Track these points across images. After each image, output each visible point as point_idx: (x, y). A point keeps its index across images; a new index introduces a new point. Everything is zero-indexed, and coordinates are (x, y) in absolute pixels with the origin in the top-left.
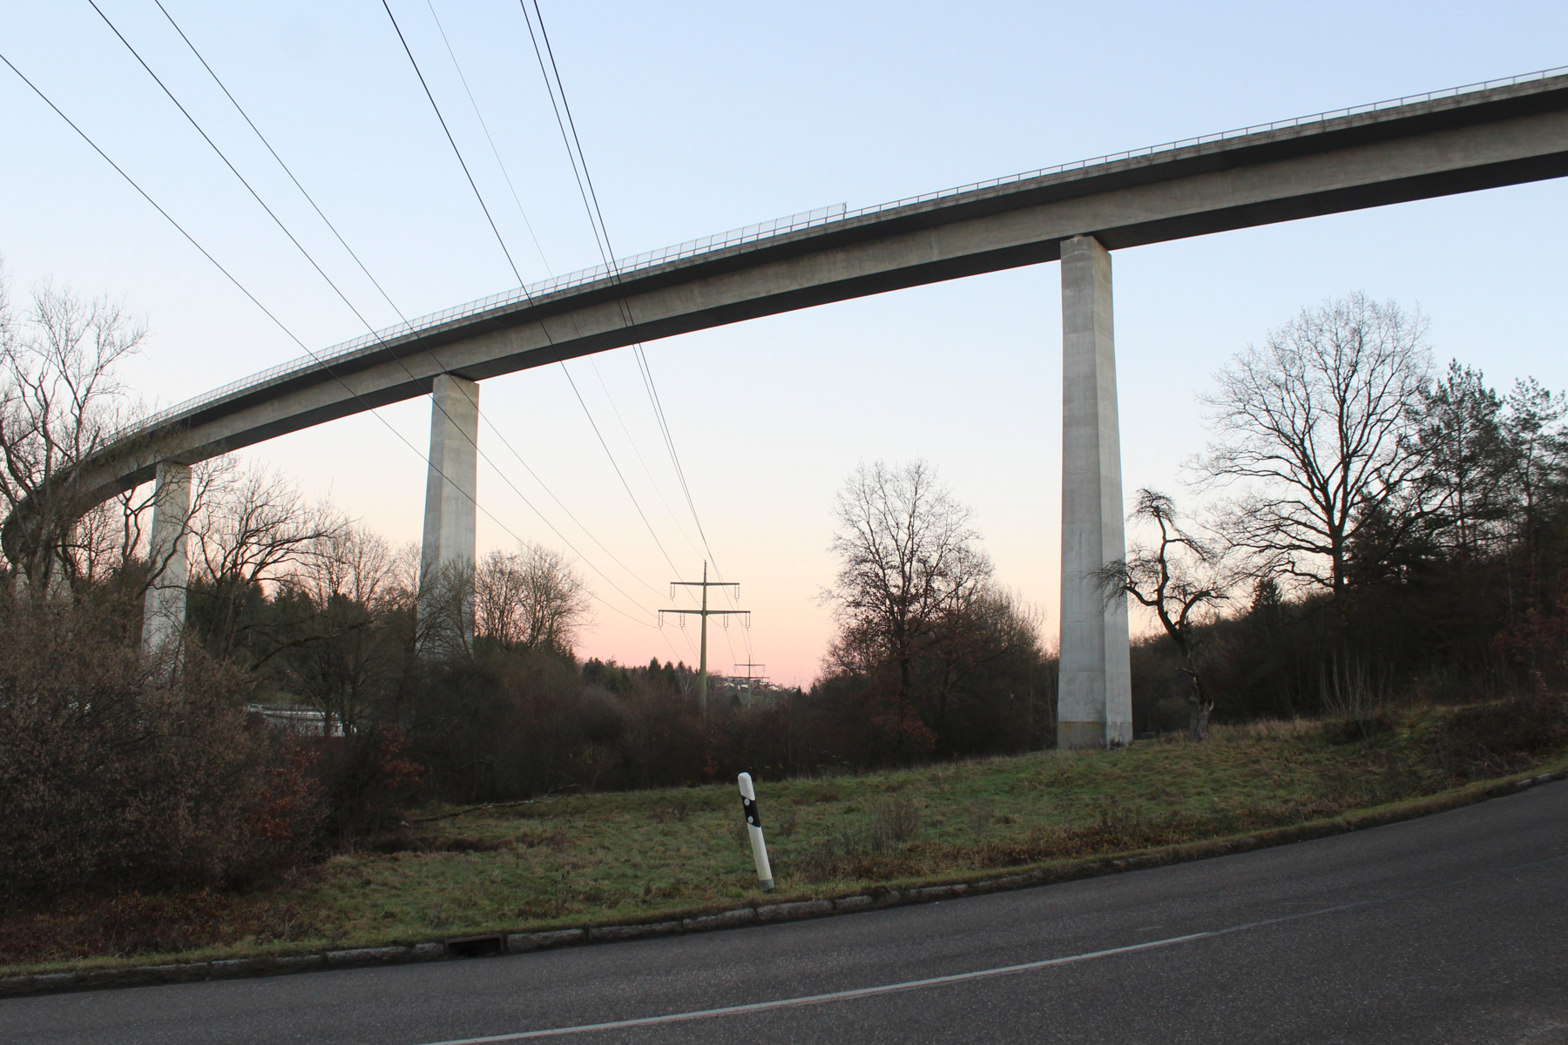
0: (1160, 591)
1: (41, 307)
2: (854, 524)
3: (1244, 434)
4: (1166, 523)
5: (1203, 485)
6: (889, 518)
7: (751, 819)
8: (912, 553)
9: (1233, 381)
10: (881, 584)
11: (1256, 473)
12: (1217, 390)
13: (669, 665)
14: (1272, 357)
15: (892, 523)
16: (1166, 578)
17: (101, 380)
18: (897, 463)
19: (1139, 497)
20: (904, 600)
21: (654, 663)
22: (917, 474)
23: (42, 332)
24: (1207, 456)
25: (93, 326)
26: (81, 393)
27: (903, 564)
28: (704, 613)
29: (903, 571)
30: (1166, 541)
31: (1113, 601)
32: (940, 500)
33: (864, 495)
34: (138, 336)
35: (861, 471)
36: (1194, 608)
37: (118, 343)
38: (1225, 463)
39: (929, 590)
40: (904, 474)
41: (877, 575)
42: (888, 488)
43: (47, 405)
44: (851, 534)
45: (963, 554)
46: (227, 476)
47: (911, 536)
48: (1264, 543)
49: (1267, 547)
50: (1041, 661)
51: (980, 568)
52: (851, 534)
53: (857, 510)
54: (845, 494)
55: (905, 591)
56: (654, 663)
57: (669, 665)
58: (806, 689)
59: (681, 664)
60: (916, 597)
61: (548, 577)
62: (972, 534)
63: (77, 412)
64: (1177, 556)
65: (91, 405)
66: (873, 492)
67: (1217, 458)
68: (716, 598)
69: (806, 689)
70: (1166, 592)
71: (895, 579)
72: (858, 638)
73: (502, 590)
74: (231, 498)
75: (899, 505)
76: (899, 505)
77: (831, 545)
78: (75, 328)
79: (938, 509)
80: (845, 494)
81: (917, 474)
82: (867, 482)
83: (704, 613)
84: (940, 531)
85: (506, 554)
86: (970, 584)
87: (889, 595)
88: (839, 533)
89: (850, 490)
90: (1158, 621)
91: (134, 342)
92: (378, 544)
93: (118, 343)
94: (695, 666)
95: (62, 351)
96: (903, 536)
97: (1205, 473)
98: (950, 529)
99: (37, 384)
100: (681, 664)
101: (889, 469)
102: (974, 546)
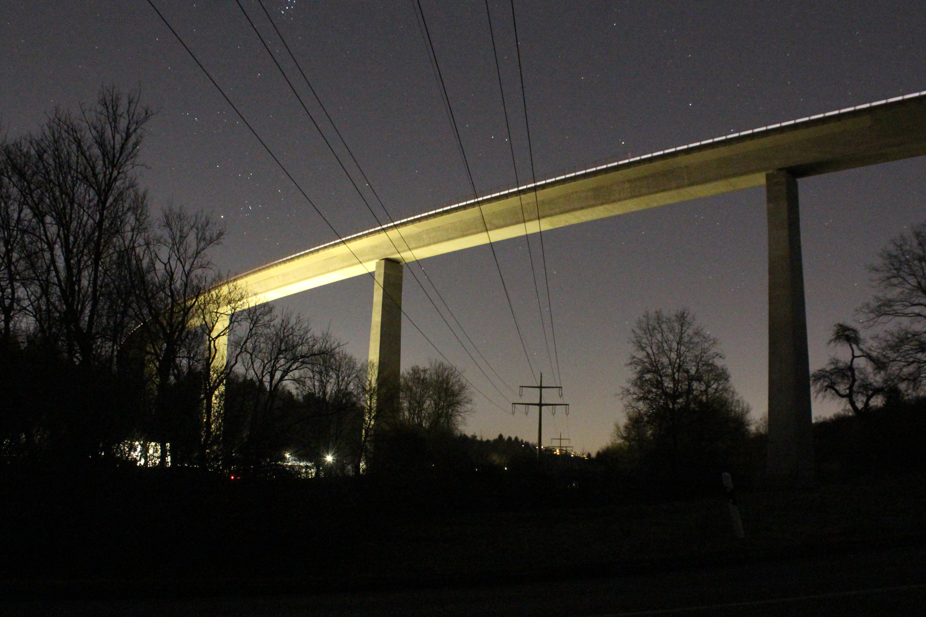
0: (851, 388)
1: (167, 217)
2: (643, 349)
3: (899, 290)
4: (854, 346)
5: (871, 323)
6: (665, 345)
7: (731, 501)
8: (680, 366)
9: (890, 256)
10: (659, 384)
11: (906, 315)
12: (879, 262)
13: (510, 438)
14: (915, 243)
15: (666, 347)
16: (854, 380)
17: (198, 261)
18: (670, 311)
19: (835, 328)
20: (674, 396)
21: (501, 436)
22: (682, 318)
23: (166, 233)
24: (874, 304)
25: (194, 229)
26: (187, 268)
27: (674, 374)
28: (540, 405)
29: (674, 378)
30: (854, 357)
31: (820, 395)
32: (697, 334)
33: (649, 331)
34: (221, 234)
35: (647, 316)
36: (872, 400)
37: (208, 238)
38: (884, 308)
39: (690, 391)
40: (674, 318)
41: (657, 380)
42: (664, 326)
43: (173, 274)
44: (641, 355)
45: (712, 367)
46: (267, 318)
47: (679, 355)
48: (911, 360)
49: (913, 362)
50: (752, 436)
51: (722, 376)
52: (641, 355)
53: (645, 340)
54: (638, 331)
55: (675, 390)
56: (501, 436)
57: (510, 438)
58: (594, 455)
59: (516, 438)
60: (680, 396)
61: (446, 380)
62: (717, 355)
63: (184, 278)
64: (862, 366)
65: (193, 275)
66: (654, 328)
67: (879, 306)
68: (550, 396)
69: (594, 455)
70: (855, 389)
71: (668, 384)
72: (636, 422)
73: (418, 390)
74: (267, 331)
75: (671, 337)
76: (671, 337)
77: (629, 362)
78: (185, 229)
79: (696, 340)
80: (638, 331)
81: (682, 318)
82: (651, 323)
83: (540, 405)
84: (697, 353)
85: (421, 367)
86: (715, 386)
87: (665, 393)
88: (634, 354)
89: (641, 328)
90: (849, 407)
91: (218, 238)
92: (350, 359)
93: (208, 238)
94: (532, 439)
95: (178, 243)
96: (673, 355)
97: (872, 315)
98: (704, 351)
99: (166, 261)
100: (516, 438)
101: (665, 314)
102: (718, 362)
